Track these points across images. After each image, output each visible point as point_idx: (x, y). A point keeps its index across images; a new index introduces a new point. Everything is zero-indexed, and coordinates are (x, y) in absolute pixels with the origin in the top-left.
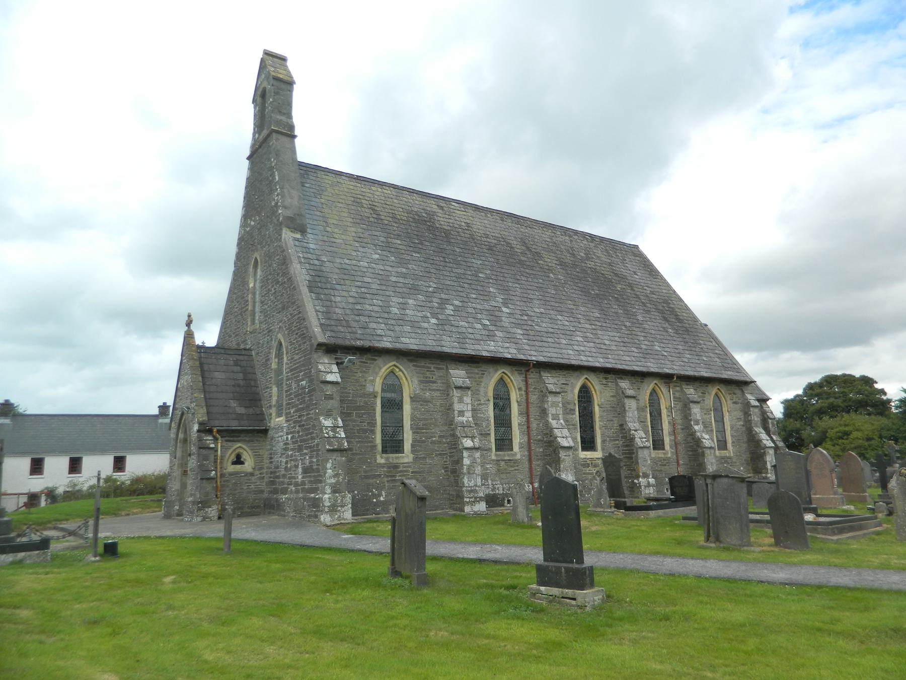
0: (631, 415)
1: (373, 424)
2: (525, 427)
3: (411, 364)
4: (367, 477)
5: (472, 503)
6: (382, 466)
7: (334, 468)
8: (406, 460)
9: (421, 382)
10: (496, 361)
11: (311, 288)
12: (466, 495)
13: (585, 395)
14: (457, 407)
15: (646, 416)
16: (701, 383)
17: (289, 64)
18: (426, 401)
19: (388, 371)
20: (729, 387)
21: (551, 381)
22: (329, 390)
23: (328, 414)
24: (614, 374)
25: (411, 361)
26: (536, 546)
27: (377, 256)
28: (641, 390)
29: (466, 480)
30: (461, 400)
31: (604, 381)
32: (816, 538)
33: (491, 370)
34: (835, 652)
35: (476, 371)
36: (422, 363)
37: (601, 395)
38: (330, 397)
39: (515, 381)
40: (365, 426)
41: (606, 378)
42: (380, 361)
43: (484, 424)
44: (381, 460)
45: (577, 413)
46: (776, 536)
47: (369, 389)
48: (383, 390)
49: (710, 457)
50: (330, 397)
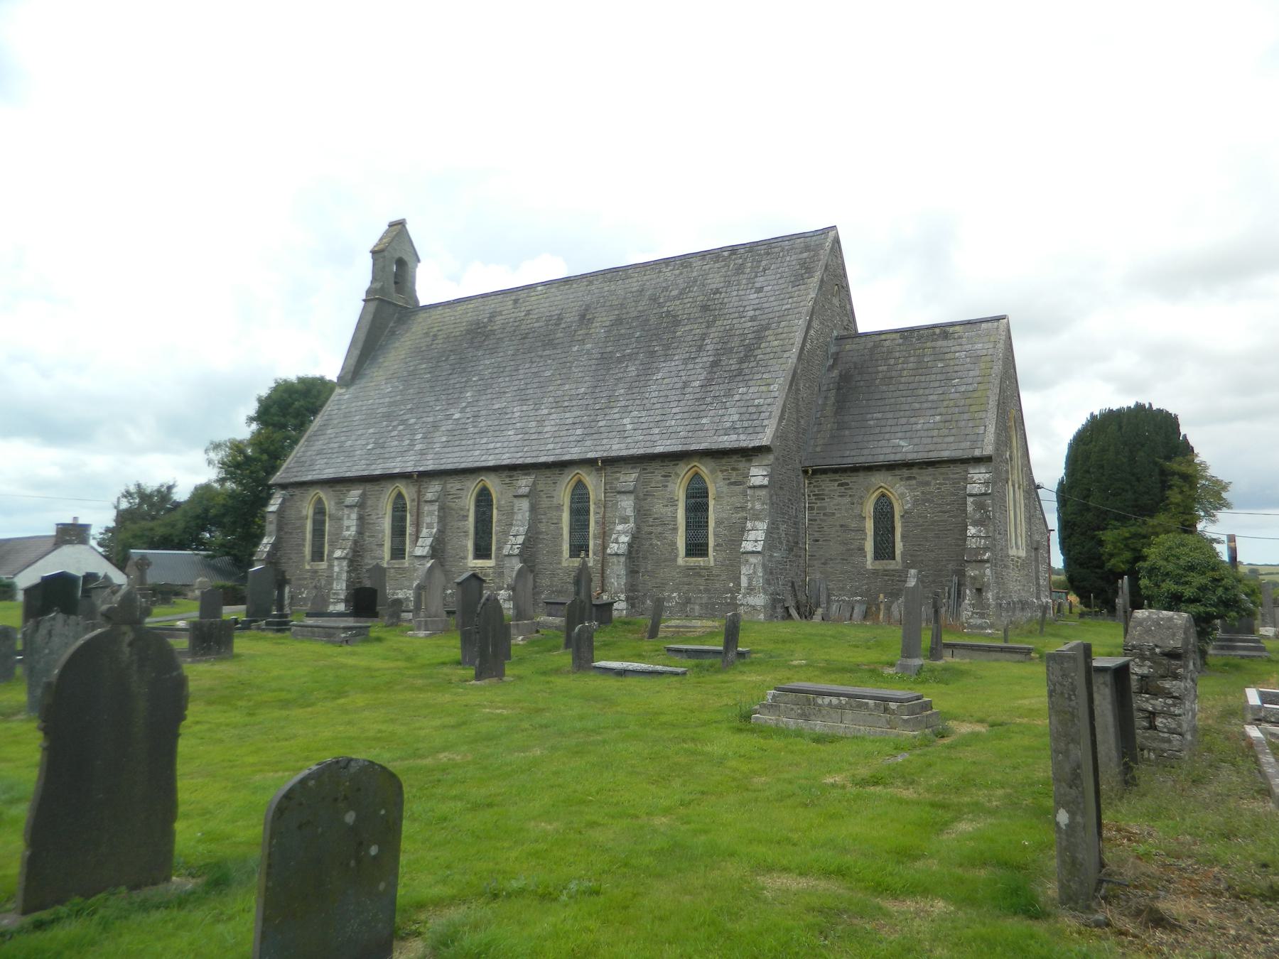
0: (520, 517)
2: (414, 537)
4: (300, 579)
5: (335, 603)
6: (308, 571)
8: (323, 567)
10: (561, 466)
12: (332, 596)
13: (484, 499)
15: (560, 518)
16: (662, 462)
17: (419, 265)
19: (476, 489)
20: (724, 461)
21: (453, 485)
24: (521, 470)
25: (331, 487)
26: (180, 653)
28: (557, 485)
29: (335, 585)
30: (349, 518)
31: (507, 480)
33: (389, 485)
34: (945, 951)
35: (377, 488)
36: (338, 488)
37: (715, 483)
39: (408, 491)
41: (510, 477)
43: (380, 535)
45: (471, 519)
47: (304, 513)
49: (615, 567)
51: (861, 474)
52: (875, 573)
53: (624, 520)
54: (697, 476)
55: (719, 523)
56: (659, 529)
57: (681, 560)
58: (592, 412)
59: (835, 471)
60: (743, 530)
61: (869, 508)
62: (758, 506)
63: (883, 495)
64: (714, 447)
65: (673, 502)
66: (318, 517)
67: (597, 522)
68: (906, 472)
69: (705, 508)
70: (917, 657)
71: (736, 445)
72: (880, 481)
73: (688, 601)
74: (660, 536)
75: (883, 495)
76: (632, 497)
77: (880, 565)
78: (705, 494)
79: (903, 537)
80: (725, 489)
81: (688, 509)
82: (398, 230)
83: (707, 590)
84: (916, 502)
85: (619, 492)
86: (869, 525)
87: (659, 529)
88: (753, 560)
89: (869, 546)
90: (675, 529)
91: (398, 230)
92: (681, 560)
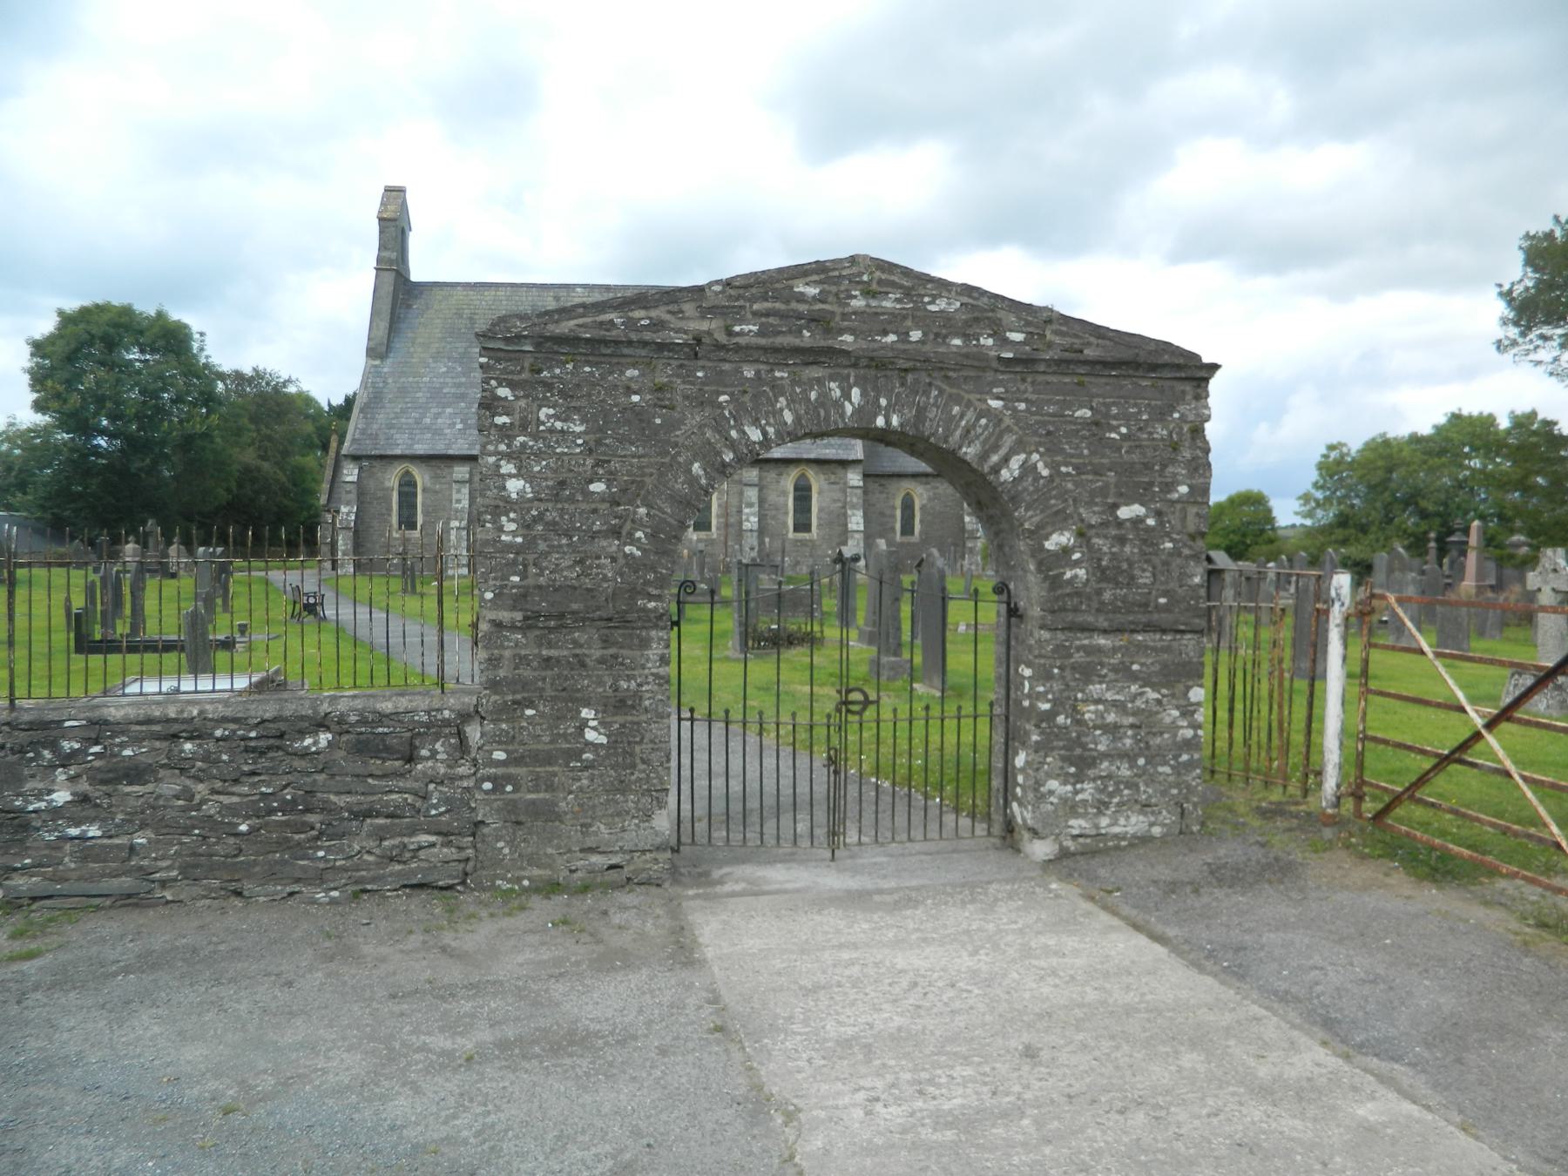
1: (390, 509)
3: (822, 477)
7: (344, 540)
9: (432, 478)
11: (362, 411)
14: (455, 496)
18: (436, 492)
22: (348, 487)
23: (348, 503)
27: (444, 369)
30: (459, 491)
32: (1469, 847)
37: (816, 481)
38: (350, 492)
40: (384, 511)
42: (396, 463)
44: (395, 535)
46: (1268, 518)
47: (387, 484)
48: (400, 485)
50: (350, 492)
51: (895, 479)
52: (902, 544)
53: (750, 505)
54: (803, 476)
55: (821, 510)
56: (774, 512)
57: (791, 535)
58: (857, 449)
59: (877, 476)
60: (845, 515)
61: (898, 503)
62: (855, 500)
63: (908, 494)
64: (822, 457)
65: (784, 493)
66: (406, 489)
67: (719, 506)
68: (924, 479)
69: (808, 499)
70: (1247, 560)
71: (835, 458)
72: (907, 485)
73: (797, 563)
74: (773, 518)
75: (908, 494)
76: (756, 489)
77: (801, 535)
78: (809, 489)
79: (921, 521)
80: (826, 487)
81: (796, 499)
82: (395, 196)
83: (811, 556)
84: (930, 499)
85: (746, 485)
86: (898, 513)
87: (774, 512)
88: (857, 536)
89: (898, 526)
90: (786, 513)
91: (395, 196)
92: (791, 535)
